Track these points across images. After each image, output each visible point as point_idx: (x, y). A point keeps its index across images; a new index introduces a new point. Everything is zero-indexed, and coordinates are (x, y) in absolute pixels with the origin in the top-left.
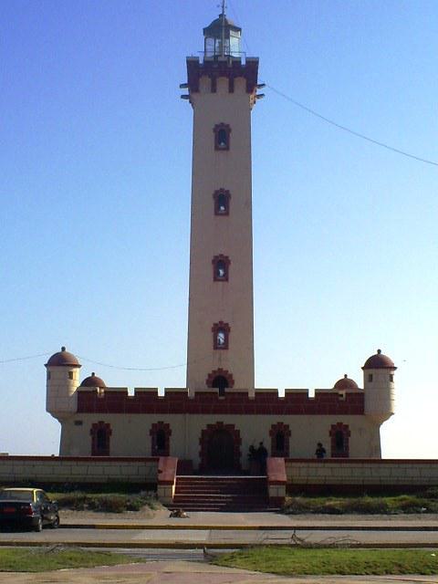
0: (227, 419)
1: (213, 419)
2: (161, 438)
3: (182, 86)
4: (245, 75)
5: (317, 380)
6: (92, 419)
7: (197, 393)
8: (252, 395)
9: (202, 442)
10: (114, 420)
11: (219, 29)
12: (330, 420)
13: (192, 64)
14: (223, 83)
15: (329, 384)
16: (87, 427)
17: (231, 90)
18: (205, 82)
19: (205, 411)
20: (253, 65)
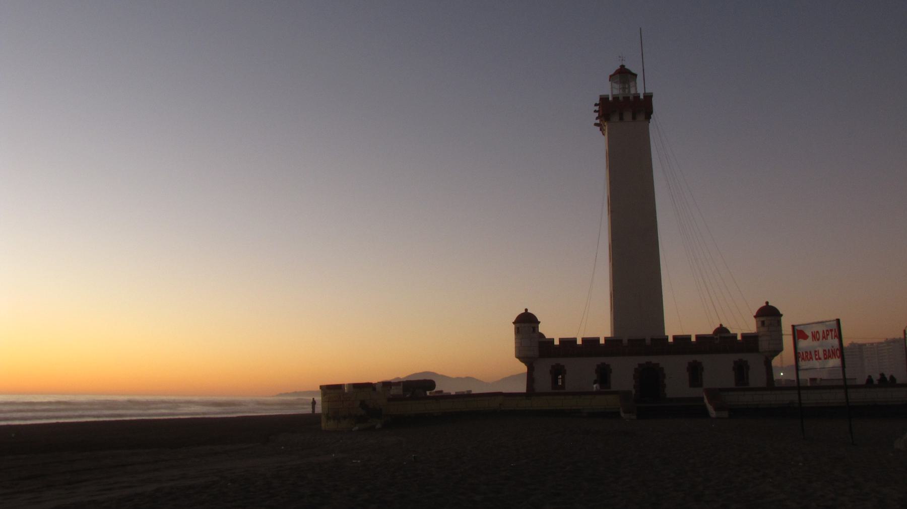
0: (653, 359)
1: (643, 360)
2: (603, 375)
3: (596, 105)
7: (652, 340)
14: (628, 116)
15: (709, 330)
20: (649, 98)
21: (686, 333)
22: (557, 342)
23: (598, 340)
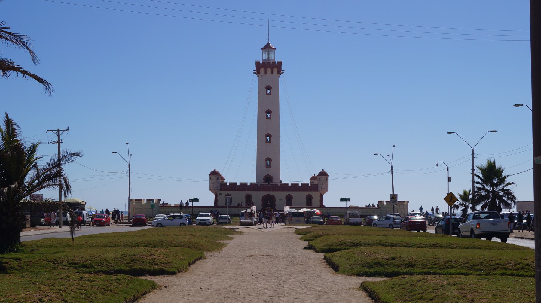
0: (271, 193)
1: (266, 193)
4: (277, 68)
5: (304, 179)
6: (224, 193)
8: (279, 185)
9: (262, 200)
10: (294, 194)
11: (267, 47)
12: (306, 193)
13: (258, 63)
14: (269, 70)
16: (224, 195)
17: (272, 73)
18: (262, 70)
19: (264, 190)
20: (280, 63)
21: (235, 182)
22: (300, 185)
23: (236, 183)
